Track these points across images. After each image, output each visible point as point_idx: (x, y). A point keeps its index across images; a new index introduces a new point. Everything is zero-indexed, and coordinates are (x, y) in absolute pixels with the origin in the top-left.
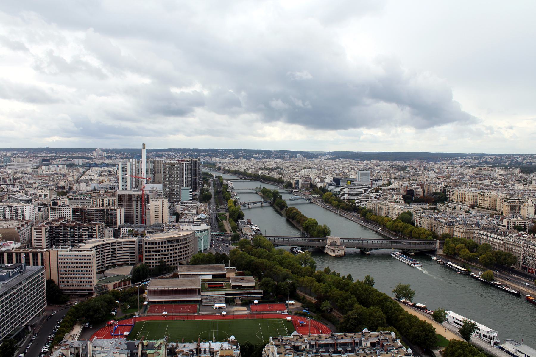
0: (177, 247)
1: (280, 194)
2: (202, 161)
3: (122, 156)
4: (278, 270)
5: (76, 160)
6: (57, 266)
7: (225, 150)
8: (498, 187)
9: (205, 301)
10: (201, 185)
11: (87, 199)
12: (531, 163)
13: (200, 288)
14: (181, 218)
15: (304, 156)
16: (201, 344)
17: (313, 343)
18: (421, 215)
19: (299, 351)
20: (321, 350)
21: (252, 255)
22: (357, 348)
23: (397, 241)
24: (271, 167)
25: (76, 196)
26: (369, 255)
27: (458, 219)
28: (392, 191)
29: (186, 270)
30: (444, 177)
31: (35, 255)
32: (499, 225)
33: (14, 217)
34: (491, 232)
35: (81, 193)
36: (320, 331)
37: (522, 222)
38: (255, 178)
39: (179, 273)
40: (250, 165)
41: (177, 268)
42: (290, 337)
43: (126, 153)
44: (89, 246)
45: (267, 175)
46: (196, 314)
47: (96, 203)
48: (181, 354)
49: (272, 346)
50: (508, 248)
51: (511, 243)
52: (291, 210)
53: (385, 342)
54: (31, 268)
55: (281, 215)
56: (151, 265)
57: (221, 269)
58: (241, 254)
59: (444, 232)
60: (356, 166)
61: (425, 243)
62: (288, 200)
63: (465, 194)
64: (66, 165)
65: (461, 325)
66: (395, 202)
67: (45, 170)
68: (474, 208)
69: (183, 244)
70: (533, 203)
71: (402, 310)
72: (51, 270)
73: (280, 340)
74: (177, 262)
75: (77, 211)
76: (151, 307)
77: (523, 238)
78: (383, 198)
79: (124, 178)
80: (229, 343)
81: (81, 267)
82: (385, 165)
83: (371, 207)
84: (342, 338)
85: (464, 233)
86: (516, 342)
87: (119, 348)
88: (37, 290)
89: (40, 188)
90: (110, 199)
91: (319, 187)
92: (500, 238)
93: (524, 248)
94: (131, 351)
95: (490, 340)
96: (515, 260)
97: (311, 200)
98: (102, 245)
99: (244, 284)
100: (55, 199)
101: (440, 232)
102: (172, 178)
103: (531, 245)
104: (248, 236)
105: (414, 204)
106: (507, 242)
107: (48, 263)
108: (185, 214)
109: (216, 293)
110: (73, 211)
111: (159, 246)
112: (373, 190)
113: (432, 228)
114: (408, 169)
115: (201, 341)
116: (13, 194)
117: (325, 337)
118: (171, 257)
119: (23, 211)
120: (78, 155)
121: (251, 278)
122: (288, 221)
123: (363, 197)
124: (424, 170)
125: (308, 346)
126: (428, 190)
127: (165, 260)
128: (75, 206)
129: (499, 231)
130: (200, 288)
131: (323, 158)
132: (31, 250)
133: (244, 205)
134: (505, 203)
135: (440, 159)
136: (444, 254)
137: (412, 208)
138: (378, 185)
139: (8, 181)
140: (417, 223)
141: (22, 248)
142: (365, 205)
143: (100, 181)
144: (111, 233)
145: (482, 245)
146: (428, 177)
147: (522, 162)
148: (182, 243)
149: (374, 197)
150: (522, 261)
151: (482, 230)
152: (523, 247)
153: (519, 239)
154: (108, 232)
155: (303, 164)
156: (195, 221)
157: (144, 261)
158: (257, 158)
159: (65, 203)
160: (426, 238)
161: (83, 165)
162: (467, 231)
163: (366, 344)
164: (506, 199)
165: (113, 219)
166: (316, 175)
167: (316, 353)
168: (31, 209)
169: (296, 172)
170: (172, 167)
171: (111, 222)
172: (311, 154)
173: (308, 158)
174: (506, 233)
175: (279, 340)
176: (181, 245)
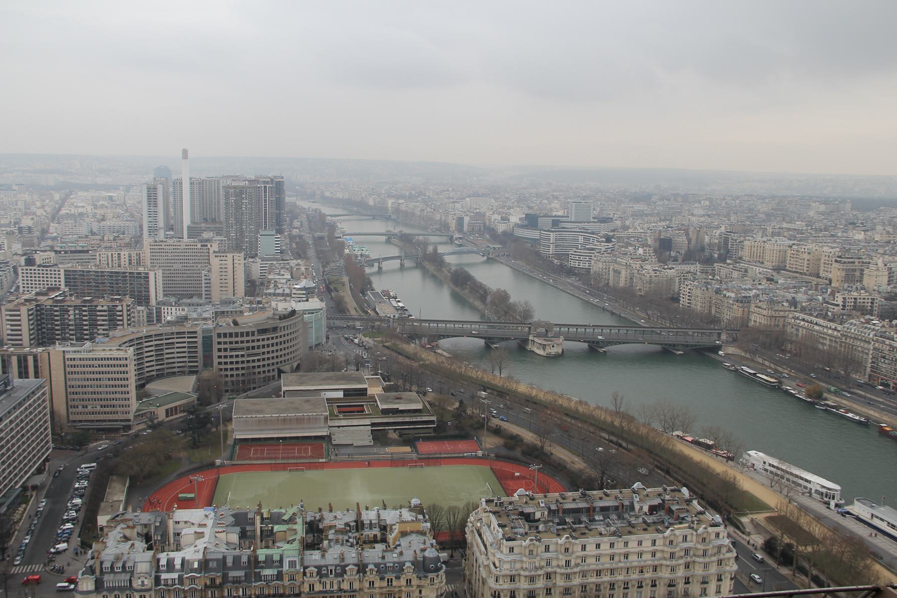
6: (63, 376)
8: (820, 235)
11: (90, 252)
18: (691, 284)
26: (604, 351)
28: (632, 239)
32: (828, 303)
37: (868, 299)
39: (284, 389)
42: (513, 499)
45: (403, 208)
48: (333, 531)
49: (486, 514)
50: (846, 343)
51: (853, 336)
53: (673, 504)
57: (360, 380)
62: (448, 254)
70: (885, 265)
76: (240, 448)
77: (873, 327)
81: (109, 380)
83: (599, 268)
84: (601, 498)
86: (873, 500)
87: (223, 524)
90: (132, 252)
92: (833, 325)
93: (874, 344)
94: (241, 528)
96: (852, 362)
99: (402, 407)
101: (727, 316)
103: (888, 339)
104: (391, 320)
106: (845, 333)
109: (355, 422)
110: (65, 275)
111: (231, 339)
118: (264, 359)
122: (457, 298)
125: (546, 513)
126: (697, 239)
129: (829, 314)
134: (837, 265)
137: (672, 271)
140: (683, 298)
143: (98, 216)
146: (693, 215)
149: (602, 251)
150: (869, 365)
152: (873, 343)
153: (866, 328)
156: (294, 294)
159: (49, 260)
162: (773, 313)
163: (641, 508)
164: (838, 257)
165: (204, 278)
166: (492, 209)
167: (558, 524)
169: (456, 202)
171: (142, 299)
174: (841, 317)
175: (496, 503)
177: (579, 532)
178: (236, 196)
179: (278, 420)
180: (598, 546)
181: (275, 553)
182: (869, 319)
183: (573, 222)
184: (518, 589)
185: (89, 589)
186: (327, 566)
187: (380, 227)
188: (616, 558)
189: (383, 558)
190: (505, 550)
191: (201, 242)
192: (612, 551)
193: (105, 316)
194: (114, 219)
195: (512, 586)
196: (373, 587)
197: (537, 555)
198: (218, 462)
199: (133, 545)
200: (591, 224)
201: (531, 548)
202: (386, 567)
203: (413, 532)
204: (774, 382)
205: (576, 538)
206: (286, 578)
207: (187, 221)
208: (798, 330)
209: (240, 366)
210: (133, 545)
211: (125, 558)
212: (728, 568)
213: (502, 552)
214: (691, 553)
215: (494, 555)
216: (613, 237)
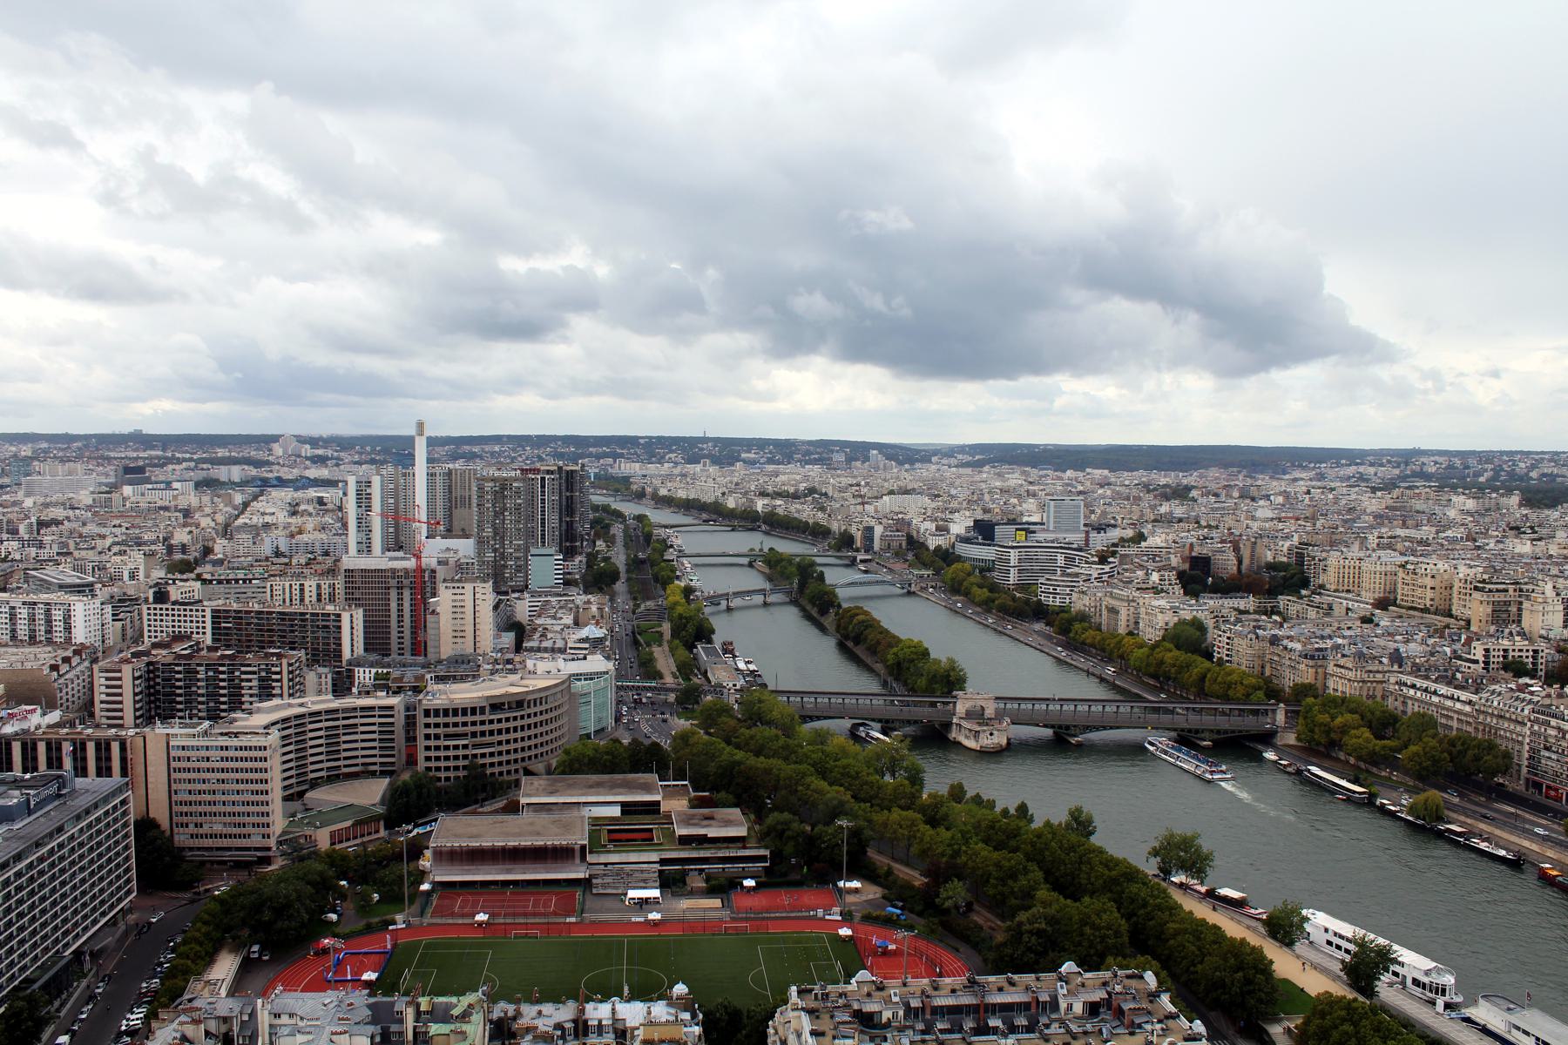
0: (519, 723)
1: (819, 569)
2: (592, 471)
3: (357, 458)
4: (815, 791)
5: (224, 468)
6: (167, 779)
7: (659, 439)
8: (1458, 547)
9: (598, 881)
10: (587, 540)
11: (254, 582)
12: (1552, 477)
13: (586, 842)
14: (530, 638)
15: (890, 458)
16: (589, 1007)
17: (917, 1005)
18: (1231, 629)
19: (874, 1027)
20: (940, 1026)
21: (738, 747)
22: (1044, 1020)
23: (1162, 705)
24: (792, 490)
25: (222, 572)
26: (1080, 745)
27: (1340, 641)
28: (1145, 558)
29: (544, 790)
30: (1298, 519)
31: (103, 747)
32: (1460, 658)
33: (41, 635)
34: (1436, 679)
35: (236, 565)
36: (935, 970)
37: (1528, 651)
38: (746, 520)
39: (523, 801)
40: (731, 482)
41: (517, 783)
42: (850, 988)
43: (368, 449)
44: (259, 720)
45: (780, 511)
46: (573, 920)
47: (279, 595)
48: (529, 1037)
49: (796, 1013)
50: (1485, 725)
51: (1496, 713)
52: (852, 613)
53: (1126, 1001)
54: (91, 785)
55: (822, 629)
56: (443, 775)
57: (647, 788)
58: (706, 744)
59: (1299, 680)
60: (1042, 487)
61: (1243, 710)
62: (842, 586)
63: (1360, 568)
64: (192, 484)
65: (1347, 951)
66: (1157, 591)
67: (132, 499)
68: (1387, 610)
69: (535, 714)
70: (1558, 594)
71: (1175, 908)
72: (149, 791)
73: (820, 996)
74: (517, 766)
75: (225, 617)
76: (440, 898)
77: (1529, 697)
78: (1122, 581)
79: (364, 521)
80: (669, 1005)
81: (238, 783)
82: (1127, 483)
83: (1085, 605)
84: (1000, 989)
85: (1358, 682)
86: (1511, 1000)
87: (347, 1019)
88: (109, 849)
89: (116, 549)
90: (323, 582)
91: (932, 548)
92: (1464, 696)
93: (1532, 726)
94: (382, 1028)
95: (1433, 996)
96: (1506, 762)
97: (910, 585)
98: (297, 717)
99: (712, 832)
100: (162, 581)
101: (1288, 680)
102: (504, 520)
103: (1554, 716)
104: (725, 691)
105: (1212, 598)
106: (1482, 708)
107: (140, 769)
108: (540, 625)
109: (633, 857)
110: (213, 617)
111: (465, 719)
112: (1093, 556)
113: (1262, 667)
114: (1194, 493)
115: (588, 1000)
116: (37, 569)
117: (950, 987)
118: (500, 753)
119: (67, 619)
120: (228, 454)
121: (736, 813)
122: (842, 647)
123: (1062, 575)
124: (1241, 497)
125: (901, 1013)
126: (1252, 556)
127: (481, 761)
128: (219, 603)
129: (1459, 676)
130: (586, 842)
131: (945, 461)
132: (90, 731)
133: (714, 600)
134: (1477, 595)
135: (1288, 464)
136: (1300, 744)
137: (1205, 608)
138: (1105, 541)
139: (22, 529)
140: (1219, 653)
141: (65, 727)
142: (1068, 601)
143: (293, 528)
144: (323, 683)
145: (1410, 718)
146: (1253, 518)
147: (1527, 474)
148: (532, 710)
149: (1093, 577)
150: (1526, 763)
151: (1410, 674)
152: (1529, 724)
153: (1517, 699)
154: (316, 680)
155: (885, 480)
156: (571, 648)
157: (422, 765)
158: (752, 463)
159: (191, 594)
160: (1247, 698)
161: (244, 483)
162: (1365, 676)
163: (1070, 1007)
164: (1479, 582)
166: (924, 514)
167: (923, 1032)
168: (92, 612)
169: (867, 503)
170: (503, 488)
171: (325, 651)
172: (909, 449)
173: (900, 463)
174: (1479, 681)
175: (816, 994)
176: (529, 716)
182: (1526, 684)
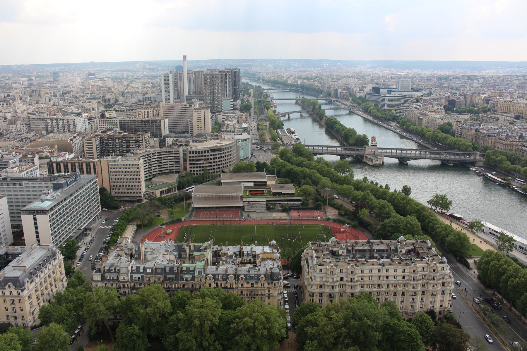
0: (220, 156)
4: (318, 178)
14: (223, 128)
16: (244, 247)
19: (337, 256)
20: (358, 256)
22: (392, 255)
24: (310, 77)
25: (122, 108)
30: (488, 87)
35: (126, 105)
36: (356, 238)
39: (222, 181)
40: (289, 74)
41: (220, 176)
42: (328, 243)
46: (239, 219)
47: (140, 115)
48: (225, 257)
49: (311, 251)
53: (420, 250)
56: (196, 173)
57: (262, 177)
58: (282, 162)
62: (327, 110)
76: (196, 212)
80: (270, 247)
84: (378, 245)
89: (87, 101)
91: (358, 96)
97: (350, 109)
99: (284, 192)
104: (288, 145)
108: (226, 123)
109: (258, 199)
110: (120, 122)
118: (214, 166)
121: (291, 185)
125: (345, 251)
132: (84, 160)
137: (453, 119)
139: (58, 95)
143: (144, 93)
146: (472, 86)
154: (154, 142)
157: (189, 169)
160: (466, 149)
162: (509, 143)
163: (401, 251)
167: (352, 258)
170: (213, 78)
171: (156, 133)
177: (361, 263)
178: (210, 79)
179: (216, 197)
180: (371, 271)
181: (192, 266)
183: (400, 91)
184: (324, 292)
185: (98, 280)
186: (218, 275)
187: (293, 95)
188: (381, 278)
189: (249, 271)
190: (318, 271)
191: (189, 104)
192: (379, 274)
193: (134, 143)
194: (152, 94)
195: (321, 291)
196: (243, 287)
197: (335, 274)
198: (183, 219)
199: (120, 259)
200: (409, 92)
201: (332, 270)
202: (250, 276)
203: (268, 259)
204: (506, 183)
205: (358, 266)
206: (197, 280)
207: (186, 93)
208: (523, 153)
209: (202, 169)
210: (120, 259)
211: (116, 265)
212: (448, 287)
213: (315, 272)
214: (426, 278)
215: (311, 273)
216: (421, 99)
